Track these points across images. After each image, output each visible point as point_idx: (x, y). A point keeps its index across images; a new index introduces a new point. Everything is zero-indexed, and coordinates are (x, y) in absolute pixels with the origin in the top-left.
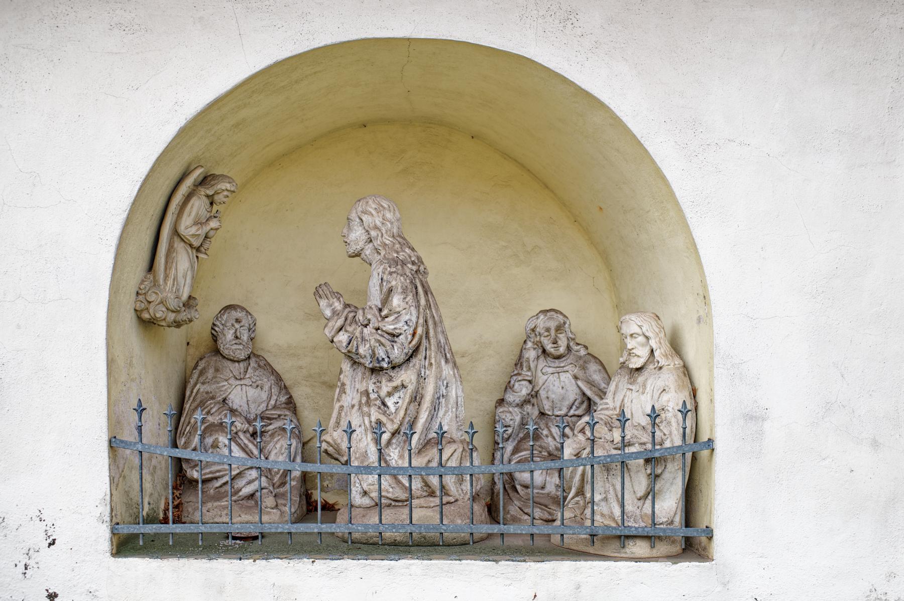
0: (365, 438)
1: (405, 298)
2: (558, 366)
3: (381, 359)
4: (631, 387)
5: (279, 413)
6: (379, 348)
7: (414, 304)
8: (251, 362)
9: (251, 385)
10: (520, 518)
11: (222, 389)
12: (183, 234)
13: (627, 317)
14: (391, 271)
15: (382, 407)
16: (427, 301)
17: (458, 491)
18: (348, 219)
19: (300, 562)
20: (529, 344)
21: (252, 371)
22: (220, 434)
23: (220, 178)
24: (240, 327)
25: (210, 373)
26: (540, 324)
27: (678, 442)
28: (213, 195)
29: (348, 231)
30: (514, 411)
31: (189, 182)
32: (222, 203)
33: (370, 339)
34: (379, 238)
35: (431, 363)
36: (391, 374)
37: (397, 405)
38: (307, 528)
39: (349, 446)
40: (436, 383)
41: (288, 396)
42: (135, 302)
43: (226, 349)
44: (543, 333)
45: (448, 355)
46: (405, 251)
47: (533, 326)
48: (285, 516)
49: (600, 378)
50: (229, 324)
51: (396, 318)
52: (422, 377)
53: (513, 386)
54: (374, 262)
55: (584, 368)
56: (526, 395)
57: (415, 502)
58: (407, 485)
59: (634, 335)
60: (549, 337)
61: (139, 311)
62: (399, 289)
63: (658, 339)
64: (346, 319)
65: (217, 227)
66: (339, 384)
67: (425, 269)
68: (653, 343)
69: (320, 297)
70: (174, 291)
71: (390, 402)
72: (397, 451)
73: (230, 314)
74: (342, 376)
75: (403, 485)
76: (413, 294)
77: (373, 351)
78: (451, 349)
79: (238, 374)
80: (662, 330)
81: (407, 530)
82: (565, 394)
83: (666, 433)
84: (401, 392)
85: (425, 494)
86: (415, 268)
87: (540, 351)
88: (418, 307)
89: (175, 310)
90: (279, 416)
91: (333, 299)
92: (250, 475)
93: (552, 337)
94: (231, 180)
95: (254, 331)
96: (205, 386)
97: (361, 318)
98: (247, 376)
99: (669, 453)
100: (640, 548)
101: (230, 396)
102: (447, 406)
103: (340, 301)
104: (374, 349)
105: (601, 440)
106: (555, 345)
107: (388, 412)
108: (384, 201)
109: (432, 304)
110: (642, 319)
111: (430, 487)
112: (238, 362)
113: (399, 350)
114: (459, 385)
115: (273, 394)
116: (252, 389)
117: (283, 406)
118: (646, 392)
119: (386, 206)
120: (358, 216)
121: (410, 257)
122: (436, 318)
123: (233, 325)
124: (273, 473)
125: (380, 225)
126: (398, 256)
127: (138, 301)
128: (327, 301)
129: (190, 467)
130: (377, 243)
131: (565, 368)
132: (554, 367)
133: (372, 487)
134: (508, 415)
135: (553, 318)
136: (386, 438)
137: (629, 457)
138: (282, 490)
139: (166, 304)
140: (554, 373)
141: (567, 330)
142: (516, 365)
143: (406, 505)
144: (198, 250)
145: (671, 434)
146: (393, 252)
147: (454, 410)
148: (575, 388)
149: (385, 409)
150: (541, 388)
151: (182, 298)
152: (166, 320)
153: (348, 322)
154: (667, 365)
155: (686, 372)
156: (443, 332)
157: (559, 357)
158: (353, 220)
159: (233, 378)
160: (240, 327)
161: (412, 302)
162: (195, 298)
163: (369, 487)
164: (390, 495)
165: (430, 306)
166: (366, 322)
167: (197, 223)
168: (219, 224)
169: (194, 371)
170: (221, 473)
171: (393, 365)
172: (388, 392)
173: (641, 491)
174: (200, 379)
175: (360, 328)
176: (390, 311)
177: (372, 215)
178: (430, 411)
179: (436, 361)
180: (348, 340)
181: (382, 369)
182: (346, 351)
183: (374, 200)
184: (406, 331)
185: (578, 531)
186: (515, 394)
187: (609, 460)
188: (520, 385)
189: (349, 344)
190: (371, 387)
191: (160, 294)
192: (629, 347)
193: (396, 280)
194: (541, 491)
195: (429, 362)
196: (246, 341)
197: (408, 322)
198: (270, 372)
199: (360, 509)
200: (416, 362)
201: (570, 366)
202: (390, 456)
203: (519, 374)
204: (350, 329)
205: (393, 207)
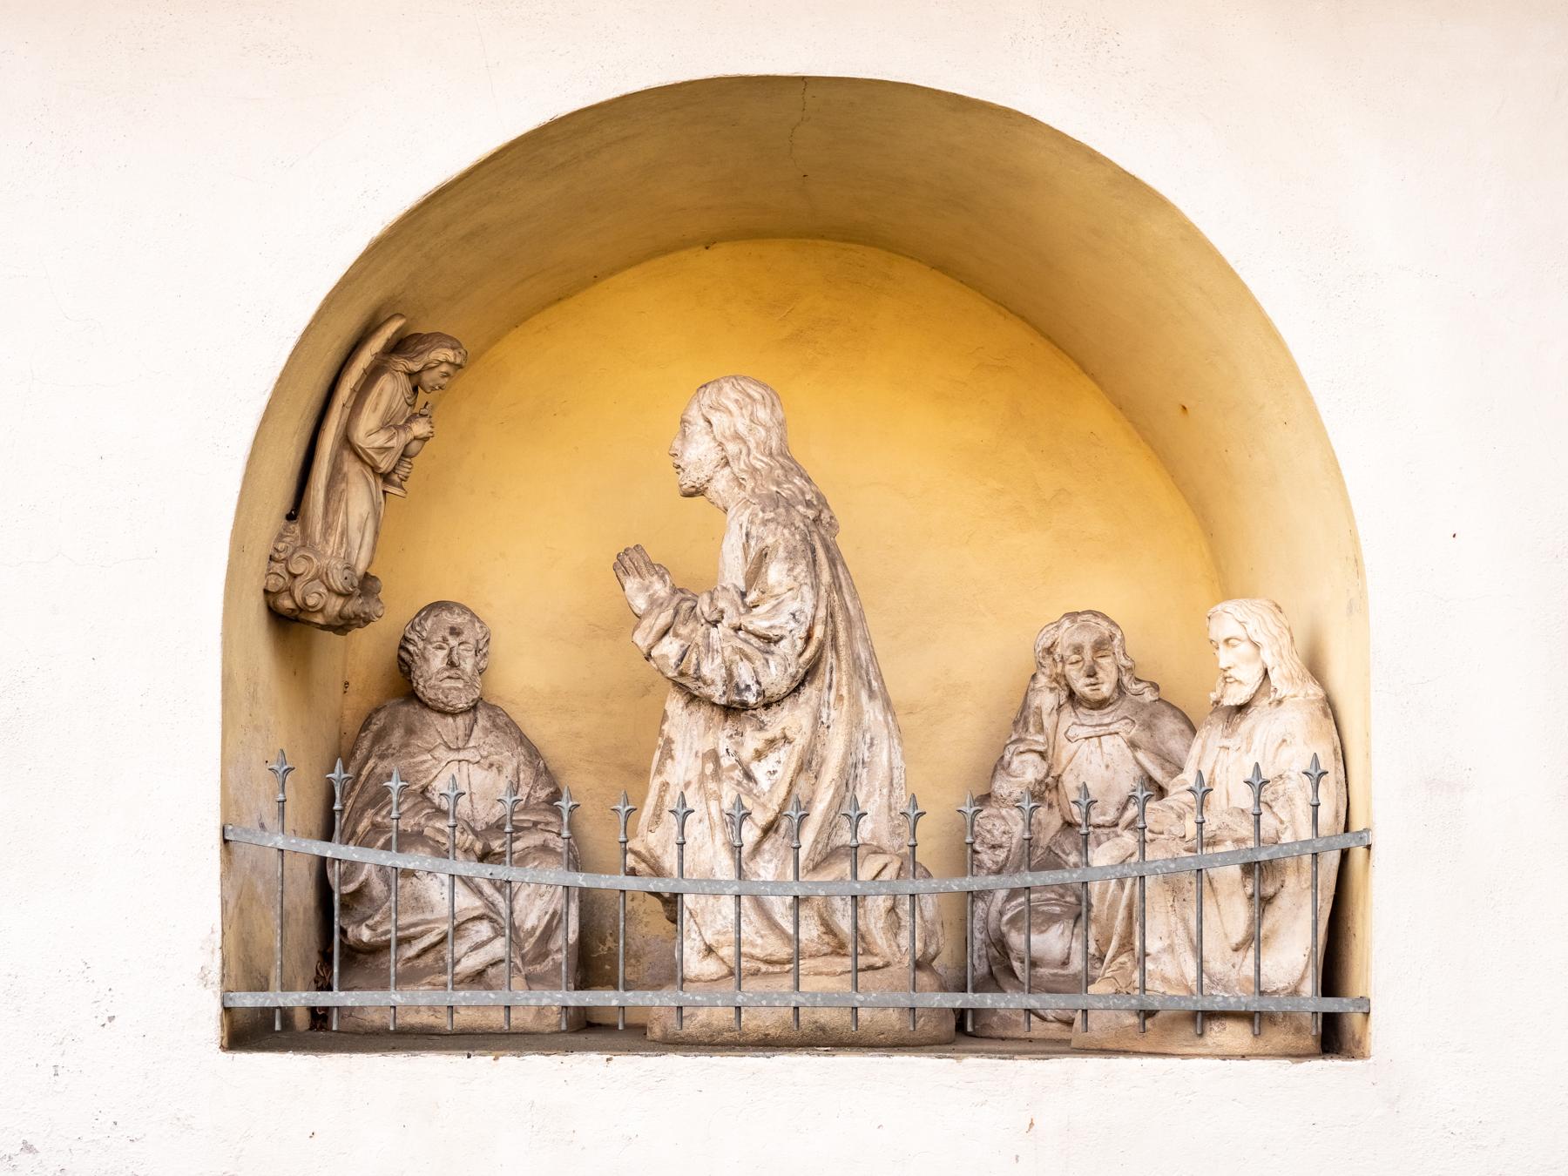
0: (709, 844)
1: (790, 570)
2: (1099, 723)
3: (743, 686)
4: (1226, 743)
5: (534, 818)
6: (741, 664)
7: (808, 581)
8: (479, 716)
9: (478, 762)
10: (1017, 1021)
11: (421, 768)
12: (362, 446)
13: (1219, 607)
14: (766, 518)
15: (745, 781)
16: (835, 577)
17: (890, 946)
18: (683, 421)
19: (583, 1061)
20: (1043, 680)
21: (481, 735)
22: (420, 848)
23: (435, 341)
24: (459, 645)
25: (396, 737)
26: (1062, 638)
27: (1306, 833)
28: (420, 371)
29: (683, 445)
30: (1010, 815)
31: (377, 344)
32: (437, 388)
33: (722, 648)
34: (743, 457)
35: (841, 695)
36: (764, 718)
37: (774, 777)
38: (598, 999)
39: (680, 840)
40: (850, 734)
41: (552, 789)
42: (266, 576)
43: (431, 688)
44: (1069, 656)
45: (874, 684)
46: (792, 482)
47: (1049, 643)
48: (546, 1017)
49: (1182, 748)
50: (437, 638)
51: (774, 607)
52: (822, 722)
53: (1009, 764)
54: (732, 505)
55: (1149, 726)
56: (1033, 781)
57: (805, 964)
58: (791, 931)
59: (1231, 641)
60: (1081, 664)
61: (273, 593)
62: (780, 553)
63: (1276, 648)
64: (676, 613)
65: (425, 435)
66: (661, 742)
67: (831, 517)
68: (1268, 657)
69: (627, 572)
70: (342, 555)
71: (759, 770)
72: (772, 866)
73: (438, 618)
74: (666, 727)
75: (783, 932)
76: (808, 562)
77: (730, 675)
78: (881, 675)
79: (452, 738)
80: (1286, 632)
81: (790, 1002)
82: (1113, 778)
83: (1284, 819)
84: (782, 752)
85: (826, 949)
86: (811, 513)
87: (1064, 694)
88: (816, 587)
89: (344, 592)
90: (535, 824)
91: (652, 576)
92: (477, 932)
93: (1087, 663)
94: (456, 344)
95: (485, 654)
96: (385, 763)
97: (706, 609)
98: (472, 743)
99: (1285, 853)
100: (1232, 1035)
101: (434, 784)
102: (870, 783)
103: (665, 582)
104: (731, 665)
105: (1162, 836)
106: (1092, 680)
107: (755, 791)
108: (752, 386)
109: (844, 584)
110: (1246, 609)
111: (835, 935)
112: (454, 714)
113: (779, 668)
114: (896, 747)
115: (521, 783)
116: (480, 770)
117: (543, 806)
118: (1253, 748)
119: (757, 396)
120: (703, 415)
121: (803, 493)
122: (852, 612)
123: (445, 640)
124: (522, 935)
125: (746, 433)
126: (779, 491)
127: (272, 573)
128: (638, 579)
129: (354, 923)
130: (738, 467)
131: (1111, 727)
132: (1091, 726)
133: (722, 938)
134: (997, 822)
135: (1089, 626)
136: (751, 840)
137: (1210, 861)
138: (538, 968)
139: (328, 579)
140: (1091, 737)
141: (1116, 650)
142: (1016, 723)
143: (788, 972)
144: (386, 478)
145: (1293, 820)
146: (770, 483)
147: (885, 791)
148: (1132, 766)
149: (751, 784)
150: (1064, 769)
151: (356, 569)
152: (326, 612)
153: (681, 617)
154: (1292, 697)
155: (1329, 710)
156: (866, 640)
157: (1101, 704)
158: (693, 422)
159: (443, 747)
160: (459, 645)
161: (806, 576)
162: (375, 579)
163: (716, 937)
164: (757, 952)
165: (840, 586)
166: (715, 616)
167: (388, 424)
168: (430, 429)
169: (363, 735)
170: (420, 929)
171: (766, 701)
172: (757, 751)
173: (1238, 935)
174: (376, 748)
175: (704, 627)
176: (763, 593)
177: (730, 412)
178: (837, 789)
179: (850, 692)
180: (681, 653)
181: (745, 706)
182: (676, 674)
183: (733, 385)
184: (793, 632)
185: (1114, 1003)
186: (1012, 779)
187: (1172, 866)
188: (1022, 762)
189: (682, 660)
190: (724, 744)
191: (315, 560)
192: (1223, 665)
193: (775, 535)
194: (1061, 972)
195: (837, 694)
196: (470, 674)
197: (797, 614)
198: (516, 740)
199: (698, 984)
200: (811, 693)
201: (1123, 722)
202: (759, 876)
203: (1019, 740)
204: (683, 631)
205: (771, 398)
